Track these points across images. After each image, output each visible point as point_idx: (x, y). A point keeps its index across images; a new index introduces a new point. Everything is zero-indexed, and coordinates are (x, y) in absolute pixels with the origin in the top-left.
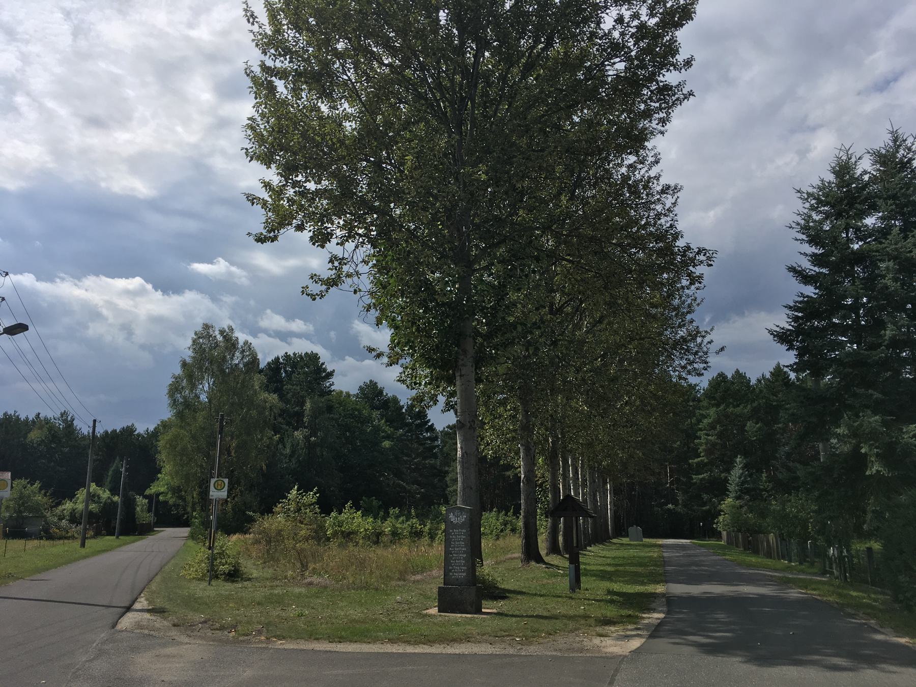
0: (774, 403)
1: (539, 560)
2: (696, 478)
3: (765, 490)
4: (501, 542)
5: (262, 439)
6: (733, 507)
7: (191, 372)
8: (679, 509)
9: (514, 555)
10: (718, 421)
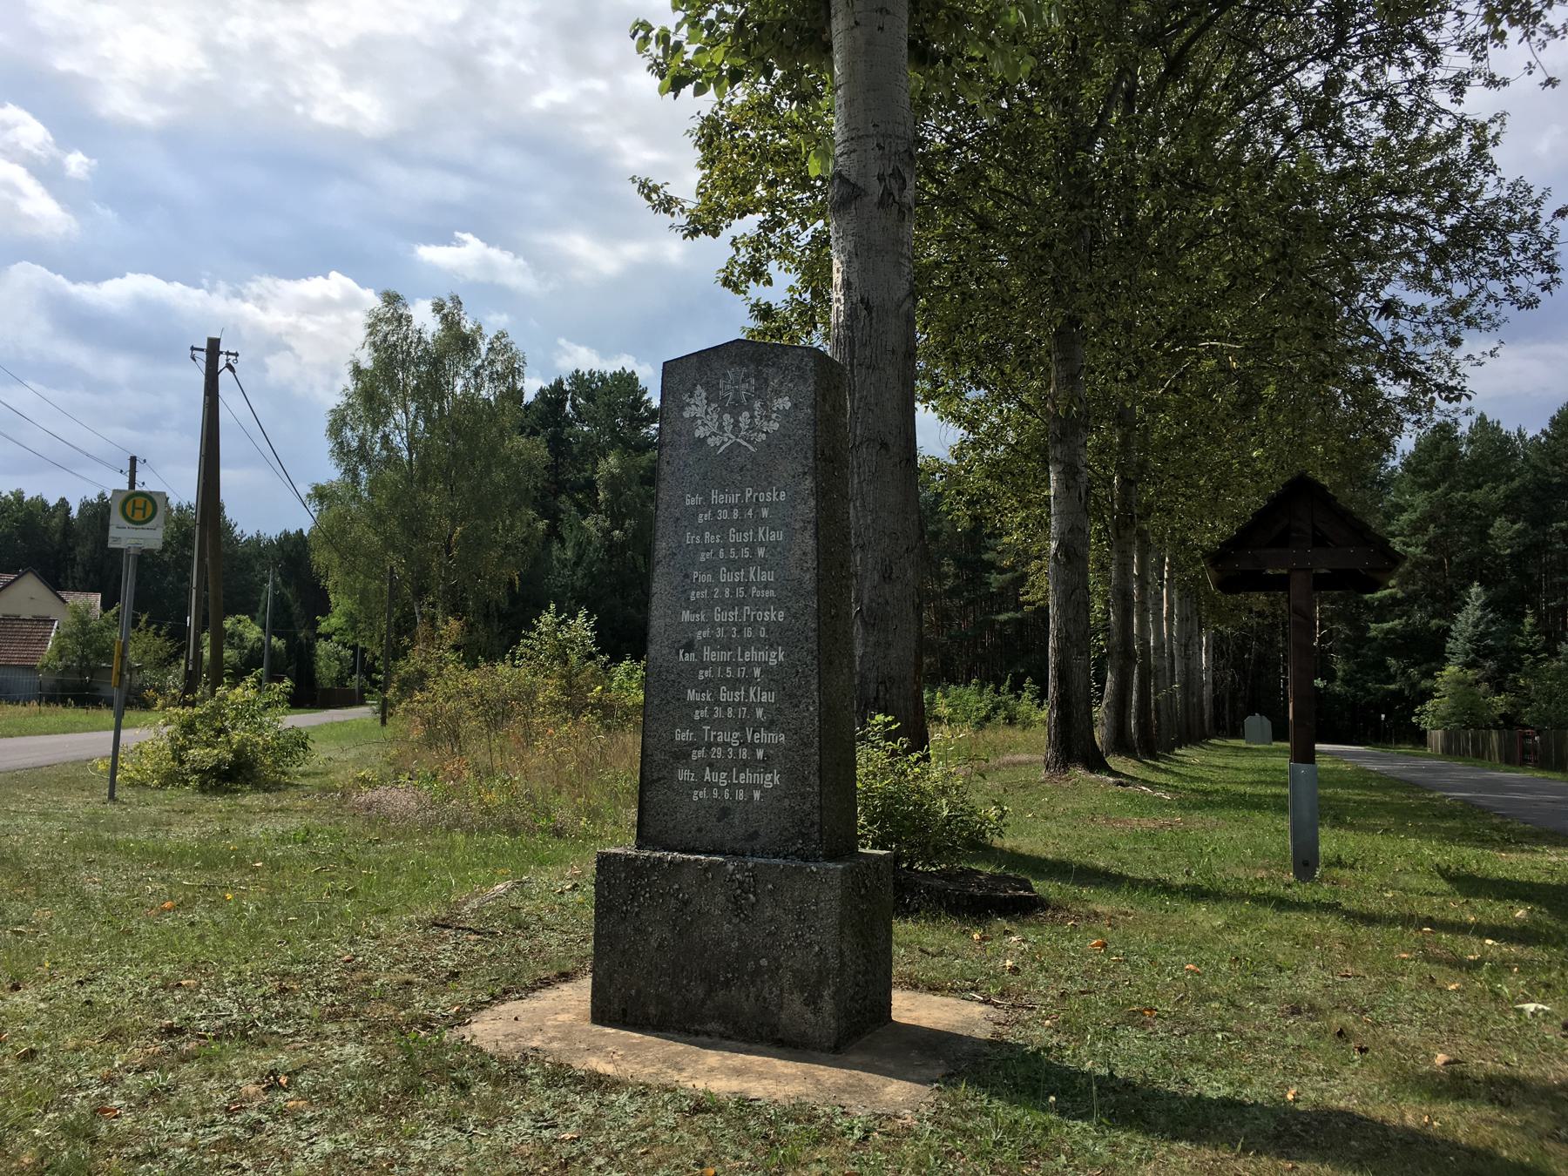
0: (1555, 480)
1: (1095, 763)
2: (1375, 629)
3: (1529, 651)
4: (989, 734)
5: (512, 526)
6: (1459, 682)
7: (371, 394)
8: (1337, 687)
9: (1018, 758)
10: (1430, 517)
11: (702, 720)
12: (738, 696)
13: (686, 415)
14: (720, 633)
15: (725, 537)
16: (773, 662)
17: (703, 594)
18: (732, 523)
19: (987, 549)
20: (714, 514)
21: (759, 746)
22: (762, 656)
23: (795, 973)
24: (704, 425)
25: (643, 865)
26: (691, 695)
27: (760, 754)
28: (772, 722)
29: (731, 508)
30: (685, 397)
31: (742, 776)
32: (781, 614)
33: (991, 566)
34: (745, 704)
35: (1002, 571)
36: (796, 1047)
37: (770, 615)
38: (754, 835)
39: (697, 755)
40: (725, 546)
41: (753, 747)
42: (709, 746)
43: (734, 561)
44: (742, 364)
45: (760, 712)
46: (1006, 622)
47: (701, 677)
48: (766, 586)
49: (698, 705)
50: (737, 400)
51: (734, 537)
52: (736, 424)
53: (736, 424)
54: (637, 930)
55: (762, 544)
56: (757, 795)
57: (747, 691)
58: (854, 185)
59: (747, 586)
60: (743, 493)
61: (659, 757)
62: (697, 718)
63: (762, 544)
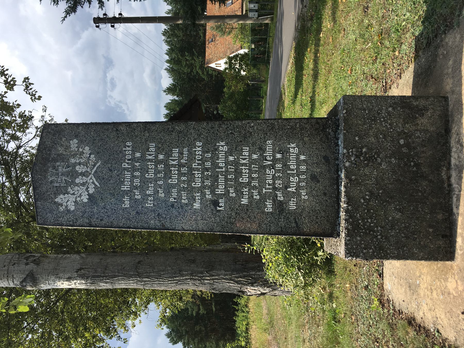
11: (260, 194)
12: (245, 170)
13: (72, 208)
14: (208, 183)
15: (150, 181)
16: (225, 148)
17: (184, 194)
18: (142, 176)
19: (192, 314)
20: (136, 188)
21: (274, 156)
22: (221, 155)
23: (405, 122)
24: (80, 196)
25: (351, 224)
26: (245, 201)
27: (279, 156)
28: (260, 149)
29: (133, 177)
30: (61, 209)
31: (292, 167)
32: (198, 144)
33: (198, 313)
34: (250, 166)
35: (199, 309)
36: (448, 121)
37: (198, 150)
38: (326, 158)
39: (281, 198)
40: (156, 180)
41: (275, 160)
42: (275, 189)
43: (165, 174)
44: (46, 171)
45: (255, 156)
46: (216, 308)
47: (234, 195)
48: (181, 153)
49: (251, 197)
50: (67, 174)
51: (151, 175)
52: (83, 174)
53: (83, 174)
54: (392, 228)
55: (156, 157)
56: (302, 157)
57: (243, 165)
58: (27, 275)
59: (180, 165)
60: (125, 169)
61: (282, 223)
62: (258, 197)
63: (156, 157)
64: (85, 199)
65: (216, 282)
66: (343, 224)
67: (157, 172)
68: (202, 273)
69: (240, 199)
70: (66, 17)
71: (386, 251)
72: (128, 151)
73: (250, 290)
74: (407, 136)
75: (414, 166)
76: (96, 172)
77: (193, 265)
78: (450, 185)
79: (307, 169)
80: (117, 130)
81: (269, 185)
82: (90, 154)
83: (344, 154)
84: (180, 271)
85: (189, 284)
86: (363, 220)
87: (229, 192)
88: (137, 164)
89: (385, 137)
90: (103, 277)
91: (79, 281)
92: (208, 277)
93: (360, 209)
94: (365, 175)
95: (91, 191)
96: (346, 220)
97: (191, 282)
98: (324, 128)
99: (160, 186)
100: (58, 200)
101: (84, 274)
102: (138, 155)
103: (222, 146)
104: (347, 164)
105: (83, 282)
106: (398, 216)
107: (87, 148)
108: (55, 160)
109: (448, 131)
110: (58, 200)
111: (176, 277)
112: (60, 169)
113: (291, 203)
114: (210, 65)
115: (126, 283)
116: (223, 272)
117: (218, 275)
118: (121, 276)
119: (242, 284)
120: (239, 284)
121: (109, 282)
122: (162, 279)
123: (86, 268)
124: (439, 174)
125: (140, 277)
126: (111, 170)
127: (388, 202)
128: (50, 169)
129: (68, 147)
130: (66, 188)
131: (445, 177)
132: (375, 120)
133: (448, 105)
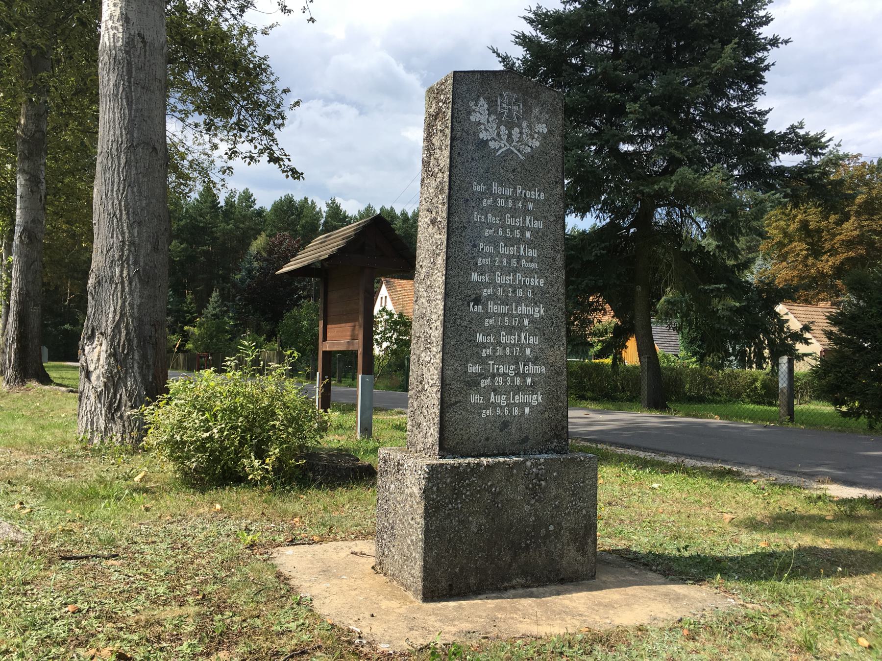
11: (488, 356)
12: (513, 339)
16: (537, 315)
17: (487, 261)
18: (509, 210)
20: (495, 201)
21: (528, 375)
23: (571, 530)
26: (480, 338)
27: (529, 381)
28: (536, 358)
29: (507, 198)
30: (472, 104)
31: (517, 397)
32: (542, 281)
34: (518, 345)
36: (572, 582)
38: (526, 440)
39: (484, 383)
41: (524, 376)
42: (493, 376)
45: (528, 351)
47: (487, 324)
49: (484, 346)
50: (510, 116)
52: (510, 135)
53: (510, 135)
54: (461, 522)
55: (528, 229)
56: (527, 410)
59: (519, 258)
60: (515, 188)
61: (456, 385)
63: (528, 229)
64: (483, 135)
65: (116, 288)
66: (451, 461)
67: (512, 228)
68: (136, 263)
69: (482, 331)
70: (498, 55)
71: (434, 516)
72: (533, 194)
73: (97, 350)
74: (557, 534)
75: (526, 544)
76: (512, 152)
77: (149, 247)
78: (506, 589)
79: (515, 416)
80: (557, 183)
81: (498, 369)
82: (531, 147)
83: (539, 459)
84: (140, 224)
85: (112, 237)
86: (468, 485)
87: (489, 318)
88: (520, 205)
89: (557, 507)
90: (129, 82)
91: (120, 35)
92: (129, 274)
93: (480, 482)
94: (517, 486)
95: (492, 144)
96: (469, 463)
97: (116, 241)
98: (557, 436)
99: (496, 232)
100: (482, 101)
101: (134, 47)
102: (530, 206)
103: (539, 311)
104: (529, 464)
105: (120, 44)
106: (474, 528)
107: (537, 144)
108: (525, 103)
109: (562, 581)
110: (482, 101)
111: (128, 214)
112: (515, 108)
113: (477, 397)
114: (384, 286)
115: (114, 121)
116: (137, 302)
117: (131, 293)
118: (130, 114)
119: (114, 336)
120: (113, 331)
121: (118, 92)
122: (124, 188)
123: (145, 51)
124: (517, 575)
125: (128, 148)
126: (514, 171)
127: (489, 515)
128: (515, 96)
129: (539, 120)
130: (496, 114)
131: (514, 582)
132: (573, 494)
133: (588, 580)
